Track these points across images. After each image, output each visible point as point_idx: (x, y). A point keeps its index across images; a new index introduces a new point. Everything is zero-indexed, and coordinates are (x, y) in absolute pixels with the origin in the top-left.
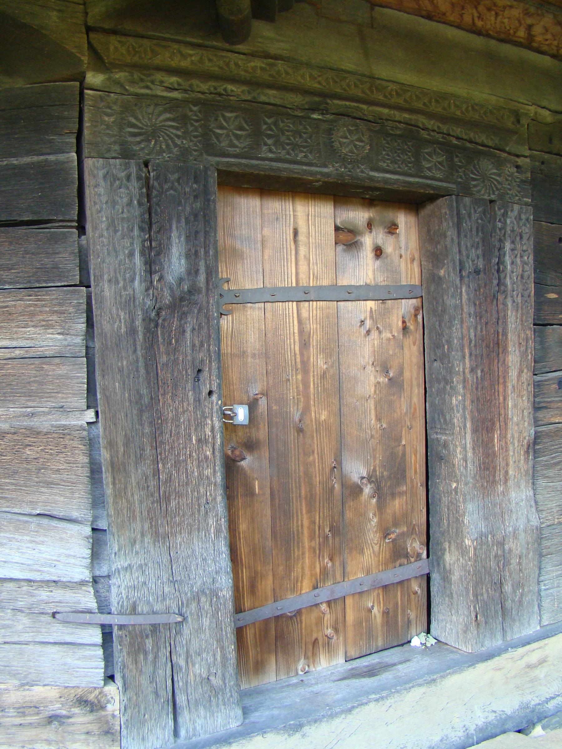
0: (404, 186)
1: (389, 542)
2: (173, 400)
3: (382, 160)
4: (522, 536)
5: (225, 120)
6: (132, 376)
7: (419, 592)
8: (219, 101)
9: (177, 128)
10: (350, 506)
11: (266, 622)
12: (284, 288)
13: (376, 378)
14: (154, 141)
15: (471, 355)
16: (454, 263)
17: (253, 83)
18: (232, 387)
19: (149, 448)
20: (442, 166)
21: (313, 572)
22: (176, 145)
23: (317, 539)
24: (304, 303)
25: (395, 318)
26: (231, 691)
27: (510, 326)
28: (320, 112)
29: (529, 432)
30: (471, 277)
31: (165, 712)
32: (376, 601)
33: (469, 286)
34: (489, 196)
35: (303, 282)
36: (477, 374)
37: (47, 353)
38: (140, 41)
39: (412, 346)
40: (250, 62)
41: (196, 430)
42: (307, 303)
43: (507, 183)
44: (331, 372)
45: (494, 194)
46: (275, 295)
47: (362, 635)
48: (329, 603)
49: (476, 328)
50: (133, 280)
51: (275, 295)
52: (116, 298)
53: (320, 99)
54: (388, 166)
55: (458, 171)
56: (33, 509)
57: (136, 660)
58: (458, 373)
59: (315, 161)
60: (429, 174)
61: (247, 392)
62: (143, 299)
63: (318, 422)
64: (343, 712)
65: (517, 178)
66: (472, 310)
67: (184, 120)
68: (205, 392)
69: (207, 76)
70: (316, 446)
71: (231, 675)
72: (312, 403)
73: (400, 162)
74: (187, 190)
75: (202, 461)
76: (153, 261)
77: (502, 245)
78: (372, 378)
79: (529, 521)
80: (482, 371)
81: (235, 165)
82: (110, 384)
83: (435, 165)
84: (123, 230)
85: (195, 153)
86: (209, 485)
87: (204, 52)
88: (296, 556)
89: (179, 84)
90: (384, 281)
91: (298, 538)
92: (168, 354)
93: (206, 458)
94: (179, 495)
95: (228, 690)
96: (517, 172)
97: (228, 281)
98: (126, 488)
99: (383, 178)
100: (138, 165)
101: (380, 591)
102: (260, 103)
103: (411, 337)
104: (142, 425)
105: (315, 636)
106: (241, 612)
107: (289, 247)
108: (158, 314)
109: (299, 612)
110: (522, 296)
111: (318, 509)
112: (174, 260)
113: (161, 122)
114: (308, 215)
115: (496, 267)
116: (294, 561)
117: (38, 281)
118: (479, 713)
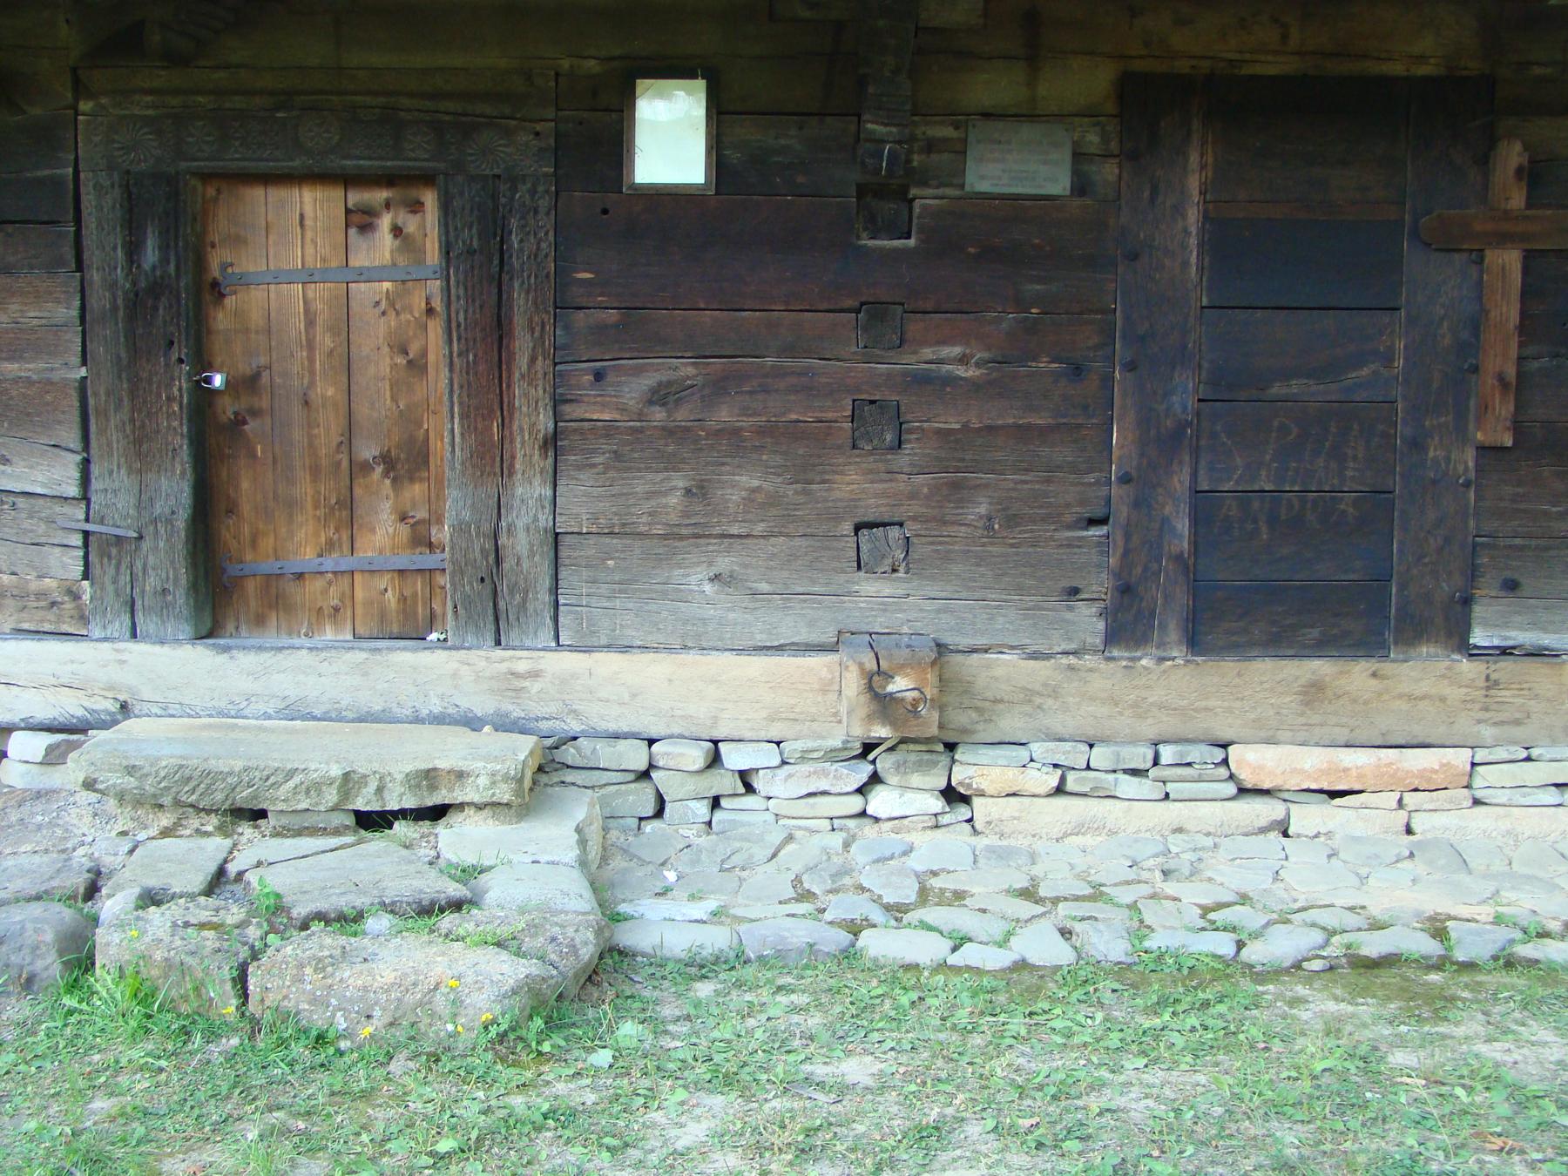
15: (459, 339)
46: (289, 277)
49: (466, 312)
60: (412, 155)
63: (323, 396)
64: (272, 648)
66: (462, 292)
68: (175, 356)
76: (133, 250)
78: (388, 360)
80: (475, 356)
82: (98, 349)
105: (319, 604)
108: (137, 295)
109: (300, 576)
118: (435, 700)
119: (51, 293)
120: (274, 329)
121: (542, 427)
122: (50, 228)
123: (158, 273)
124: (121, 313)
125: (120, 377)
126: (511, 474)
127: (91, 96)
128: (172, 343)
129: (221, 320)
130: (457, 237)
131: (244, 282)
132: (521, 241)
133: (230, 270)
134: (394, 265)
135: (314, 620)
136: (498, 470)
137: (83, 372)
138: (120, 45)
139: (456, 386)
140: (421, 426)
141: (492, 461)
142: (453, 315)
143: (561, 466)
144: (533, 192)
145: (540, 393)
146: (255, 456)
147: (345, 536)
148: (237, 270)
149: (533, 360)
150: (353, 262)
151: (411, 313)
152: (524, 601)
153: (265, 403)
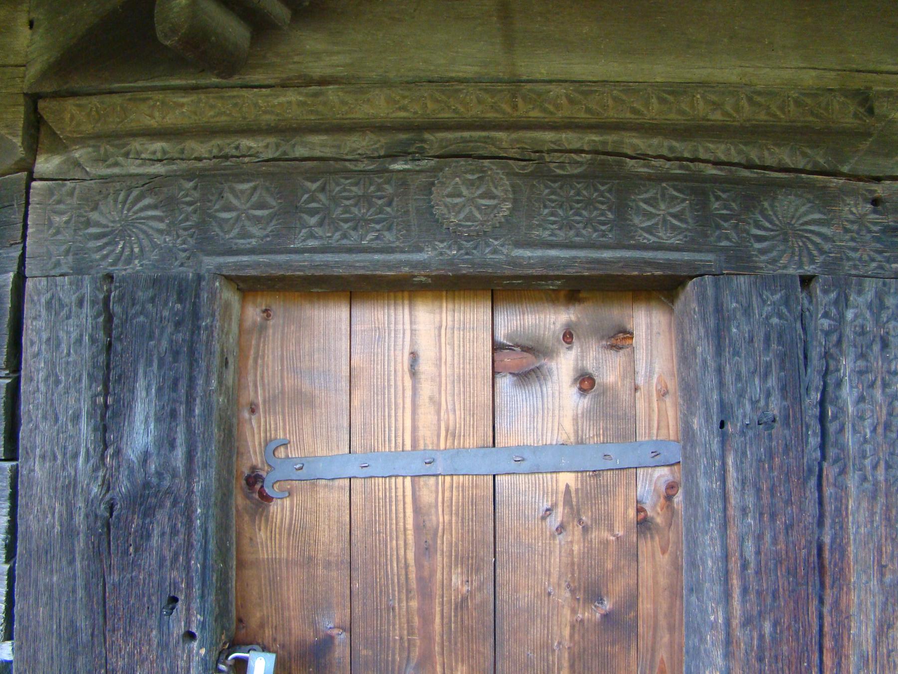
0: (589, 269)
2: (126, 642)
3: (539, 226)
5: (236, 197)
6: (64, 599)
9: (160, 219)
13: (574, 611)
14: (122, 243)
15: (745, 591)
16: (708, 409)
17: (287, 130)
18: (286, 614)
20: (681, 220)
22: (155, 246)
25: (620, 503)
27: (852, 530)
28: (410, 157)
30: (750, 433)
33: (744, 454)
34: (800, 265)
36: (761, 628)
38: (107, 99)
40: (278, 96)
42: (432, 480)
43: (847, 237)
44: (478, 598)
45: (812, 261)
49: (760, 537)
50: (76, 456)
52: (49, 482)
53: (408, 137)
55: (718, 227)
58: (713, 626)
59: (397, 243)
61: (314, 623)
62: (88, 485)
65: (875, 224)
66: (750, 501)
67: (170, 204)
68: (178, 629)
69: (208, 132)
72: (437, 649)
73: (581, 225)
74: (166, 313)
76: (109, 420)
77: (832, 364)
78: (567, 612)
80: (776, 624)
81: (248, 266)
83: (665, 221)
84: (67, 380)
85: (184, 255)
87: (203, 96)
89: (164, 152)
90: (598, 435)
96: (875, 212)
99: (541, 257)
100: (94, 280)
103: (657, 538)
107: (399, 383)
108: (111, 508)
110: (888, 467)
113: (135, 213)
114: (440, 327)
115: (817, 411)
120: (358, 561)
124: (80, 544)
127: (58, 145)
128: (174, 600)
129: (267, 541)
130: (741, 395)
132: (861, 399)
133: (281, 453)
134: (580, 442)
138: (120, 42)
142: (733, 544)
148: (293, 453)
151: (611, 529)
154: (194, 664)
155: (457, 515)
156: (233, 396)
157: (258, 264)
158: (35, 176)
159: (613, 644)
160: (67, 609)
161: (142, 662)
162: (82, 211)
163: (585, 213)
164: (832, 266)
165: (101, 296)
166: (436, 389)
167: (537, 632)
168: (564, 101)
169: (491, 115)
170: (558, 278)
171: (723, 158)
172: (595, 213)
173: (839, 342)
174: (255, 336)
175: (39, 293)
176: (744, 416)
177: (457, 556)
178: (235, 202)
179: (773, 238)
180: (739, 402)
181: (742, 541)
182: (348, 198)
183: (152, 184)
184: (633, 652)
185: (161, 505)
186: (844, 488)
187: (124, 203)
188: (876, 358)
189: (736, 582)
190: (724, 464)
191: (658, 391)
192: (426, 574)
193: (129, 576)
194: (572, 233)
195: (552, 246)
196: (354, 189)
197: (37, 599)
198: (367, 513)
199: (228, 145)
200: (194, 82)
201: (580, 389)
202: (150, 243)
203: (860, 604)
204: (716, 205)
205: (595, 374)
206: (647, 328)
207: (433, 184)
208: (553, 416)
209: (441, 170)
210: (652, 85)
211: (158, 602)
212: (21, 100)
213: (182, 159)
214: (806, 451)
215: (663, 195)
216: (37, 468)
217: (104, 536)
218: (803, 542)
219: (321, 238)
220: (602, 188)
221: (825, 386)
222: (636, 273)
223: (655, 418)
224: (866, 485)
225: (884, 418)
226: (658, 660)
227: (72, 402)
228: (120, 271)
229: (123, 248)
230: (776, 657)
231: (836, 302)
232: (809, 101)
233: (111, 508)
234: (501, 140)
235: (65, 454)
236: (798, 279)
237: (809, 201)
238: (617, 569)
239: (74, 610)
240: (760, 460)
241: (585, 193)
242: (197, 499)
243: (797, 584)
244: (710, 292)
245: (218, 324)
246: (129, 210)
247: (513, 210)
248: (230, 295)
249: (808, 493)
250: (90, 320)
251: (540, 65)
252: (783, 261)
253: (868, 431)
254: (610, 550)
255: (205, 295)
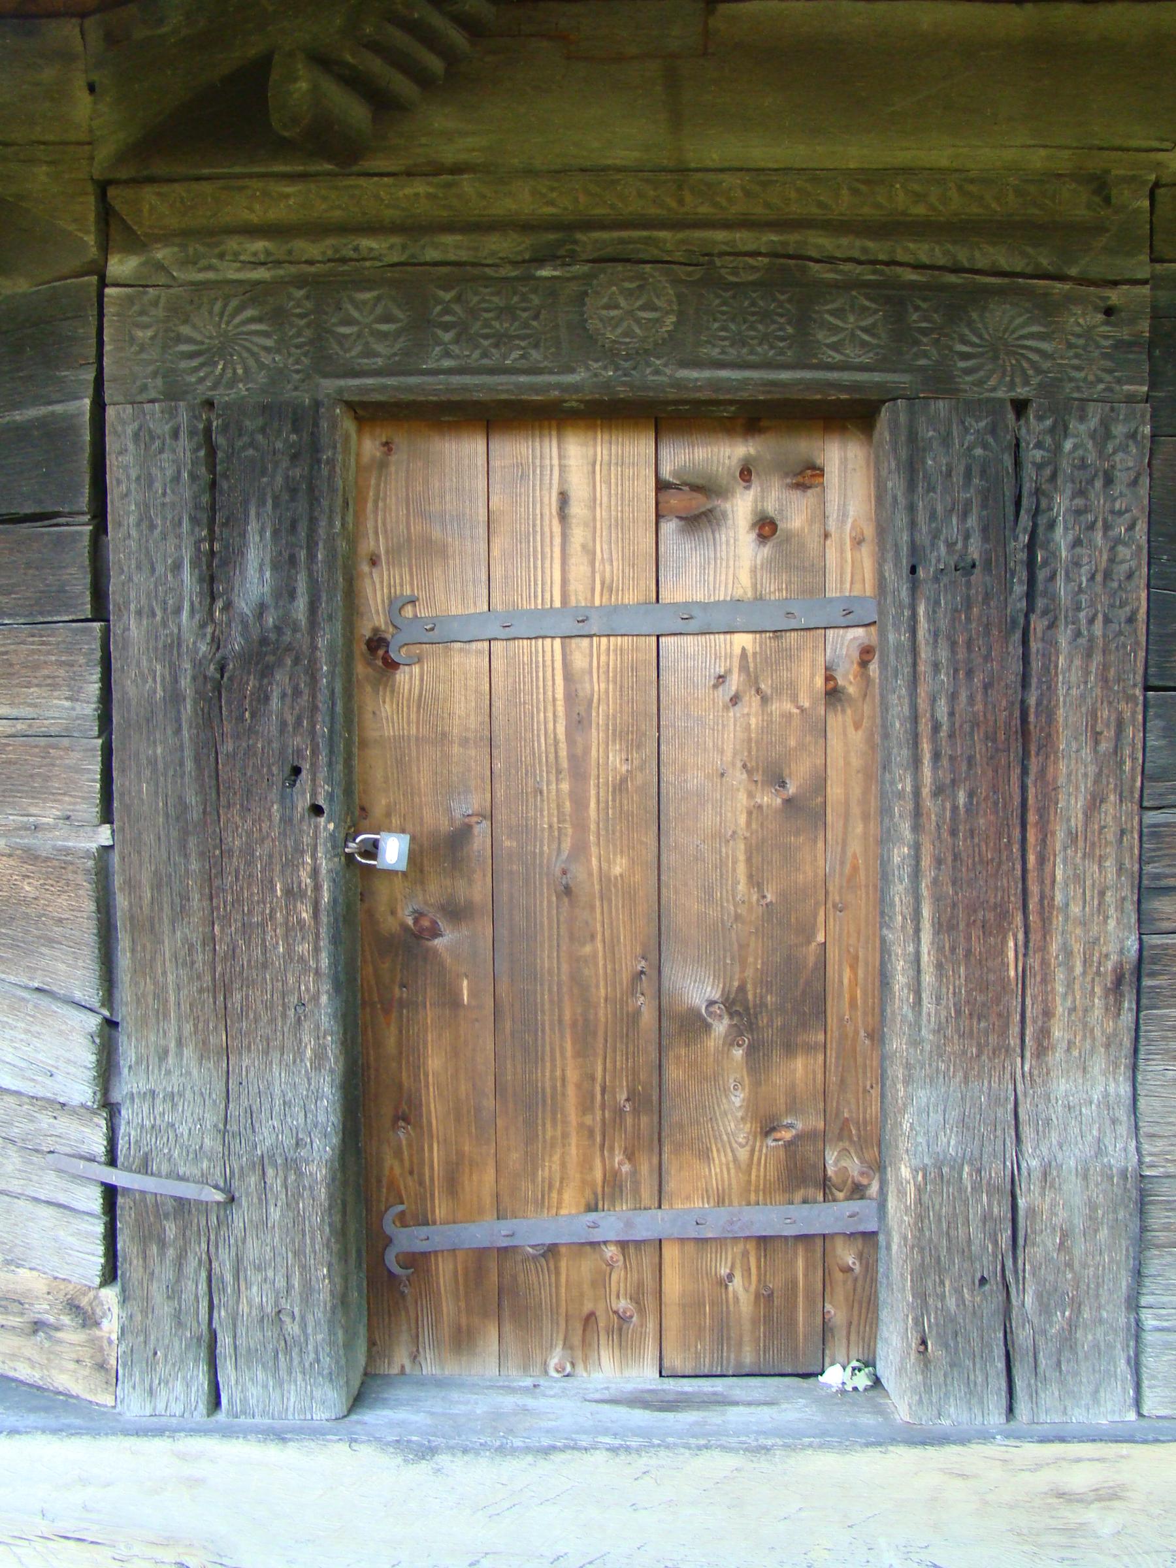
1: (777, 1147)
4: (1072, 1185)
5: (357, 308)
7: (857, 1268)
8: (343, 274)
9: (266, 334)
10: (678, 1057)
11: (481, 1253)
12: (530, 612)
13: (751, 795)
15: (936, 756)
17: (413, 228)
18: (417, 800)
19: (197, 897)
20: (873, 335)
21: (588, 1178)
22: (262, 366)
23: (599, 1113)
24: (578, 640)
25: (806, 671)
26: (317, 1353)
27: (1061, 691)
29: (1119, 940)
31: (191, 1355)
32: (738, 1265)
33: (937, 603)
34: (1012, 386)
35: (579, 597)
36: (955, 798)
37: (53, 730)
38: (195, 186)
39: (851, 729)
41: (283, 872)
43: (1071, 353)
45: (1026, 383)
46: (514, 627)
47: (701, 1329)
48: (623, 1245)
49: (953, 697)
50: (178, 611)
51: (514, 627)
52: (148, 642)
53: (556, 238)
54: (723, 352)
55: (917, 342)
56: (31, 979)
57: (145, 1252)
58: (900, 795)
61: (449, 810)
62: (195, 643)
64: (528, 1450)
65: (1106, 337)
66: (944, 654)
67: (278, 317)
68: (303, 803)
69: (317, 230)
70: (599, 926)
71: (317, 1323)
72: (592, 838)
73: (755, 342)
74: (279, 445)
75: (291, 930)
76: (215, 571)
77: (1044, 504)
78: (742, 797)
79: (1100, 1151)
80: (971, 794)
83: (853, 335)
84: (164, 525)
85: (297, 377)
86: (306, 970)
87: (313, 186)
88: (548, 1137)
91: (554, 1104)
92: (237, 737)
93: (301, 922)
94: (249, 983)
95: (310, 1347)
96: (1107, 323)
97: (413, 602)
98: (153, 959)
100: (191, 408)
101: (751, 1247)
102: (426, 264)
103: (849, 712)
104: (186, 856)
105: (588, 1307)
106: (427, 1224)
107: (547, 529)
108: (222, 669)
109: (552, 1251)
110: (1107, 621)
111: (601, 1052)
112: (252, 571)
113: (237, 327)
115: (1023, 556)
116: (544, 1148)
117: (41, 614)
119: (36, 667)
120: (500, 737)
121: (1112, 948)
122: (39, 529)
123: (270, 621)
125: (183, 846)
126: (1042, 1051)
127: (135, 243)
128: (297, 771)
129: (389, 715)
130: (935, 535)
131: (440, 636)
132: (1077, 543)
133: (408, 612)
135: (576, 1340)
136: (1014, 1042)
137: (104, 836)
138: (216, 119)
139: (926, 862)
140: (810, 939)
141: (995, 1021)
142: (923, 704)
143: (1150, 1031)
144: (1103, 435)
145: (1111, 874)
146: (455, 1003)
147: (645, 1168)
148: (423, 613)
149: (1095, 802)
150: (666, 596)
151: (794, 698)
152: (1072, 1326)
153: (478, 890)
154: (320, 841)
155: (615, 683)
156: (353, 540)
157: (384, 387)
158: (108, 281)
159: (797, 834)
160: (174, 783)
161: (263, 840)
162: (170, 324)
163: (760, 327)
164: (1049, 389)
165: (201, 426)
166: (590, 537)
167: (708, 819)
168: (739, 193)
169: (653, 211)
170: (731, 402)
171: (925, 260)
172: (773, 327)
173: (1053, 477)
174: (374, 474)
175: (124, 423)
176: (939, 561)
177: (614, 730)
178: (356, 314)
179: (982, 354)
180: (933, 545)
181: (933, 700)
182: (487, 310)
183: (254, 293)
184: (820, 844)
185: (280, 663)
186: (1054, 644)
187: (222, 314)
188: (1097, 496)
189: (926, 747)
190: (914, 616)
191: (853, 539)
192: (579, 751)
193: (244, 745)
194: (745, 350)
195: (721, 365)
196: (495, 299)
197: (139, 773)
198: (510, 680)
199: (347, 245)
200: (301, 168)
201: (760, 535)
202: (255, 363)
203: (1069, 775)
204: (915, 317)
205: (777, 518)
206: (841, 463)
207: (586, 293)
208: (727, 567)
209: (595, 276)
210: (848, 172)
211: (279, 773)
212: (90, 188)
213: (291, 263)
214: (1010, 600)
215: (852, 306)
216: (133, 626)
217: (215, 701)
218: (1004, 703)
219: (458, 357)
220: (782, 298)
221: (1035, 526)
222: (819, 397)
223: (849, 570)
224: (1080, 641)
225: (1104, 565)
226: (849, 854)
227: (171, 549)
228: (223, 396)
229: (223, 369)
230: (972, 832)
231: (1052, 430)
232: (1032, 189)
233: (222, 669)
234: (665, 241)
235: (165, 610)
236: (1009, 407)
237: (1027, 311)
238: (802, 746)
239: (183, 785)
240: (956, 610)
241: (761, 303)
242: (322, 656)
243: (997, 750)
244: (903, 418)
245: (340, 458)
246: (228, 323)
247: (677, 324)
248: (348, 425)
249: (1011, 649)
250: (188, 454)
251: (714, 148)
252: (992, 382)
253: (1084, 579)
254: (794, 724)
255: (324, 425)
